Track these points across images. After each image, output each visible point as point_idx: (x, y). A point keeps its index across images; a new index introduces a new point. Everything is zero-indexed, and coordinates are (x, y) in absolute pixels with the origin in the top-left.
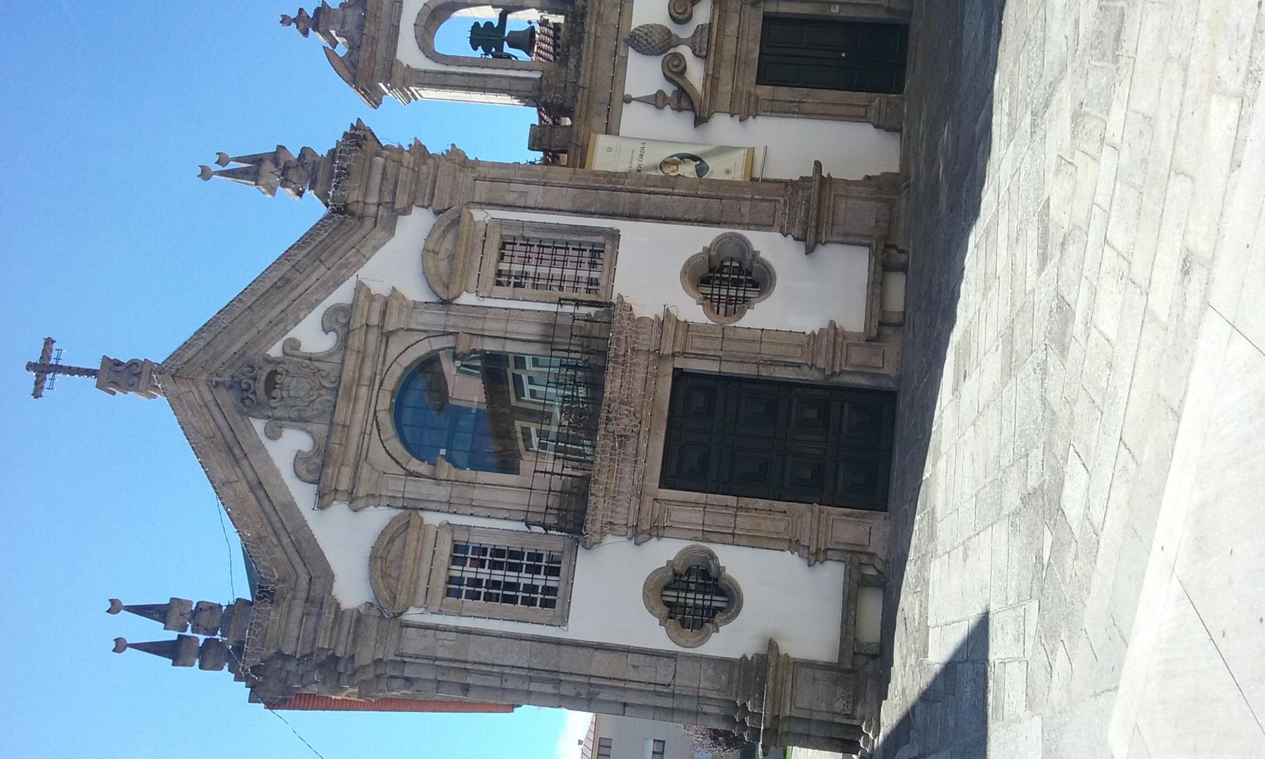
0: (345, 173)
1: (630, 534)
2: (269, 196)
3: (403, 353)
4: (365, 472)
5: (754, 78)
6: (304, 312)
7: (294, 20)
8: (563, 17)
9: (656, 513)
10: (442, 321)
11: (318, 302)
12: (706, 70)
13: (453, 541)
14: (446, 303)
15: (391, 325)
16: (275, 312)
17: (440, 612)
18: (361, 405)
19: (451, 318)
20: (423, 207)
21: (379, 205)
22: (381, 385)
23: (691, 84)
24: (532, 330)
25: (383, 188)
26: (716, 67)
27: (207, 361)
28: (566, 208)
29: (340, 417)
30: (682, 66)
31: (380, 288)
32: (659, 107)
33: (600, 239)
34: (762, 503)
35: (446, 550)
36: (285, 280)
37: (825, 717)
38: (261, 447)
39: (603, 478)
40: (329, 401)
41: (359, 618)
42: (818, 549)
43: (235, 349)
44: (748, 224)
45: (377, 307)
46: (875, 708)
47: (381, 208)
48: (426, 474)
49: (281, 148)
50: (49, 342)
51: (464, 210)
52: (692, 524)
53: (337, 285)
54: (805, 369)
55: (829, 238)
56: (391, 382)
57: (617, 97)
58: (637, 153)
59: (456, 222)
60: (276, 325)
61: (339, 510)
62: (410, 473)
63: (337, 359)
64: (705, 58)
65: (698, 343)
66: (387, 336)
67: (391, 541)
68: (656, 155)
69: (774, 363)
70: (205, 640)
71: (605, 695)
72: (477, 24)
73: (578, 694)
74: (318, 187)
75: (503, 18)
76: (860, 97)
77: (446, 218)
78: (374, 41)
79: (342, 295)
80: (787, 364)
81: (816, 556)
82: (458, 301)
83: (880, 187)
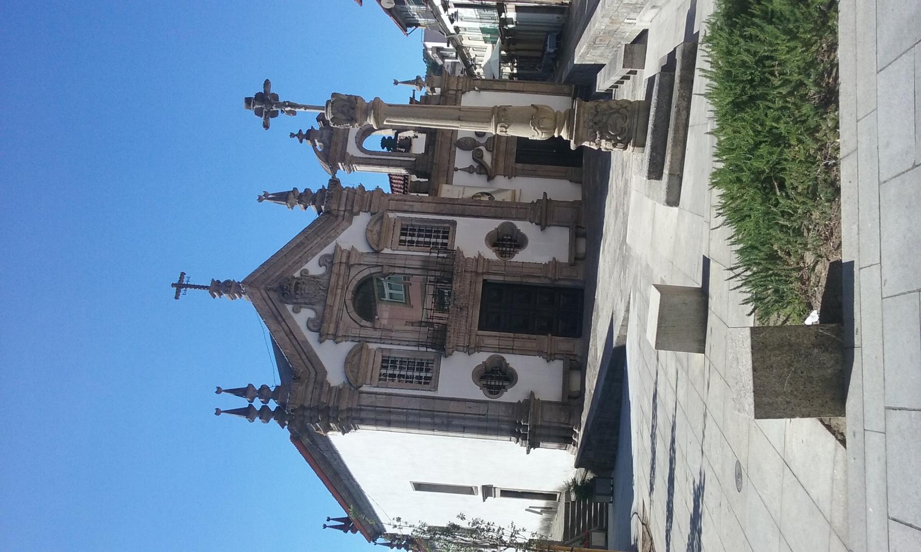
0: (330, 197)
1: (465, 350)
2: (290, 209)
3: (359, 276)
4: (341, 325)
5: (514, 160)
6: (310, 258)
7: (296, 135)
8: (425, 135)
9: (477, 340)
10: (375, 260)
11: (317, 253)
12: (492, 156)
13: (383, 357)
14: (377, 252)
15: (352, 262)
16: (297, 258)
17: (377, 387)
18: (338, 297)
19: (379, 259)
20: (366, 212)
21: (345, 211)
22: (347, 288)
23: (485, 162)
24: (417, 264)
25: (347, 204)
26: (497, 155)
27: (264, 280)
28: (431, 212)
29: (329, 302)
30: (482, 154)
31: (346, 246)
32: (471, 173)
33: (447, 225)
34: (525, 336)
35: (379, 360)
36: (302, 243)
37: (556, 425)
38: (291, 317)
39: (453, 324)
40: (323, 295)
41: (340, 391)
42: (551, 354)
43: (277, 274)
44: (515, 218)
45: (345, 254)
46: (579, 418)
47: (346, 212)
48: (369, 326)
49: (295, 189)
50: (183, 274)
51: (385, 213)
52: (494, 345)
53: (325, 246)
54: (543, 278)
55: (551, 223)
56: (352, 288)
57: (451, 169)
58: (461, 192)
59: (382, 218)
60: (297, 263)
61: (329, 343)
62: (361, 326)
63: (326, 277)
64: (491, 151)
65: (494, 268)
66: (349, 267)
67: (354, 355)
68: (469, 193)
69: (529, 276)
70: (263, 406)
71: (455, 422)
72: (384, 137)
73: (443, 422)
74: (317, 204)
75: (396, 135)
76: (562, 168)
77: (377, 217)
78: (337, 144)
79: (329, 250)
80: (534, 277)
81: (550, 357)
82: (382, 252)
83: (574, 205)
